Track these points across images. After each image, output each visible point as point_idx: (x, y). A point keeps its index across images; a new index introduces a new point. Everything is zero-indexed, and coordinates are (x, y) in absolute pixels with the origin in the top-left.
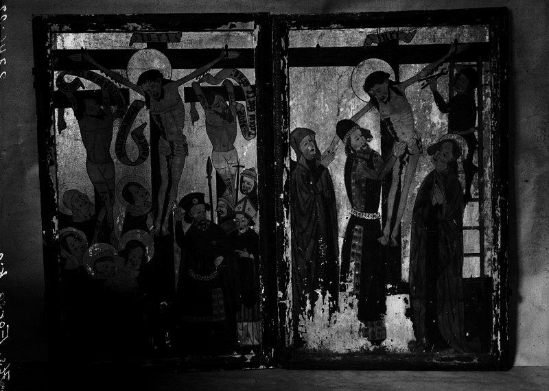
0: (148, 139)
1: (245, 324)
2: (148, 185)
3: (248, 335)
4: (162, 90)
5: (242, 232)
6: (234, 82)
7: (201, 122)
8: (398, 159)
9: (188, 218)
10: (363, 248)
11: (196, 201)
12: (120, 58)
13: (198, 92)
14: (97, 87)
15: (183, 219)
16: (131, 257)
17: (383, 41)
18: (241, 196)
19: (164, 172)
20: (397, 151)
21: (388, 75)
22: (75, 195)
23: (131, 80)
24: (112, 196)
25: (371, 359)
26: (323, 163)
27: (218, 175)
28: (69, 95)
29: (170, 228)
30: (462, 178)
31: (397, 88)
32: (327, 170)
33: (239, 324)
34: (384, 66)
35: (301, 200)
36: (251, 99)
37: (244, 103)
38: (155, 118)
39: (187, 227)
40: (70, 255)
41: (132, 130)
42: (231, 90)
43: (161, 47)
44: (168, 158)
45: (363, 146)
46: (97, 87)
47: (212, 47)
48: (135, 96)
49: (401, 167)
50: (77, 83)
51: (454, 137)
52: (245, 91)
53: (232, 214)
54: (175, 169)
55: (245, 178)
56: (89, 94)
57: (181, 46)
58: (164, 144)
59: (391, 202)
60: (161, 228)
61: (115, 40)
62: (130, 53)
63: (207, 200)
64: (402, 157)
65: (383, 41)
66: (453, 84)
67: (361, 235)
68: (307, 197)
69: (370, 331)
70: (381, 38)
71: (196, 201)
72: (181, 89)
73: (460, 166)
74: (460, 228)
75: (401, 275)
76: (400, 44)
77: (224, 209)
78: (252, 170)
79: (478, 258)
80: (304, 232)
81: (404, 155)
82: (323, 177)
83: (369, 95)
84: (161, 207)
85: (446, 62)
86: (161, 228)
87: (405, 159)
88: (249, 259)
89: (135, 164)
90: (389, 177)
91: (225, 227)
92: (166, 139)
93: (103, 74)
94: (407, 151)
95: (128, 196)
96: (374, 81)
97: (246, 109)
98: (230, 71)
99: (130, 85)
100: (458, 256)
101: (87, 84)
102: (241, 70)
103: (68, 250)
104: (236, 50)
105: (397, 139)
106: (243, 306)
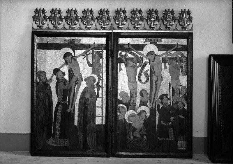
0: (149, 75)
1: (181, 142)
2: (148, 91)
3: (182, 146)
4: (155, 58)
5: (181, 108)
6: (180, 56)
7: (168, 69)
8: (74, 82)
9: (162, 103)
10: (62, 113)
11: (164, 97)
12: (140, 47)
13: (167, 59)
14: (133, 57)
15: (160, 103)
16: (141, 116)
17: (70, 42)
18: (181, 96)
19: (154, 86)
20: (74, 79)
21: (72, 54)
22: (124, 94)
23: (144, 55)
24: (136, 94)
25: (99, 154)
26: (48, 83)
27: (173, 88)
28: (123, 59)
29: (155, 106)
30: (96, 90)
31: (74, 58)
32: (50, 86)
33: (178, 142)
34: (70, 50)
35: (40, 95)
36: (185, 62)
37: (183, 63)
38: (152, 67)
39: (161, 106)
40: (121, 114)
41: (144, 71)
42: (178, 59)
43: (155, 44)
44: (156, 82)
45: (63, 78)
46: (133, 57)
47: (172, 44)
48: (145, 60)
49: (75, 85)
50: (126, 55)
51: (93, 75)
52: (183, 60)
53: (177, 103)
54: (158, 86)
55: (182, 90)
56: (131, 59)
57: (162, 43)
58: (154, 78)
60: (152, 106)
61: (140, 41)
62: (144, 45)
63: (169, 97)
64: (76, 82)
65: (70, 42)
66: (93, 57)
67: (61, 109)
68: (42, 95)
69: (63, 143)
70: (69, 41)
71: (164, 97)
72: (161, 58)
73: (95, 86)
74: (94, 106)
75: (74, 123)
76: (76, 43)
77: (174, 100)
78: (185, 87)
79: (101, 118)
80: (41, 107)
81: (76, 81)
82: (48, 88)
83: (65, 60)
84: (152, 99)
85: (91, 49)
86: (152, 106)
87: (77, 83)
88: (183, 118)
89: (144, 83)
90: (71, 88)
91: (175, 106)
92: (155, 75)
93: (135, 52)
94: (77, 80)
95: (141, 94)
96: (66, 55)
97: (183, 65)
98: (178, 52)
99: (144, 56)
100: (94, 116)
101: (130, 56)
102: (182, 52)
103: (120, 112)
104: (180, 45)
105: (74, 76)
106: (180, 135)
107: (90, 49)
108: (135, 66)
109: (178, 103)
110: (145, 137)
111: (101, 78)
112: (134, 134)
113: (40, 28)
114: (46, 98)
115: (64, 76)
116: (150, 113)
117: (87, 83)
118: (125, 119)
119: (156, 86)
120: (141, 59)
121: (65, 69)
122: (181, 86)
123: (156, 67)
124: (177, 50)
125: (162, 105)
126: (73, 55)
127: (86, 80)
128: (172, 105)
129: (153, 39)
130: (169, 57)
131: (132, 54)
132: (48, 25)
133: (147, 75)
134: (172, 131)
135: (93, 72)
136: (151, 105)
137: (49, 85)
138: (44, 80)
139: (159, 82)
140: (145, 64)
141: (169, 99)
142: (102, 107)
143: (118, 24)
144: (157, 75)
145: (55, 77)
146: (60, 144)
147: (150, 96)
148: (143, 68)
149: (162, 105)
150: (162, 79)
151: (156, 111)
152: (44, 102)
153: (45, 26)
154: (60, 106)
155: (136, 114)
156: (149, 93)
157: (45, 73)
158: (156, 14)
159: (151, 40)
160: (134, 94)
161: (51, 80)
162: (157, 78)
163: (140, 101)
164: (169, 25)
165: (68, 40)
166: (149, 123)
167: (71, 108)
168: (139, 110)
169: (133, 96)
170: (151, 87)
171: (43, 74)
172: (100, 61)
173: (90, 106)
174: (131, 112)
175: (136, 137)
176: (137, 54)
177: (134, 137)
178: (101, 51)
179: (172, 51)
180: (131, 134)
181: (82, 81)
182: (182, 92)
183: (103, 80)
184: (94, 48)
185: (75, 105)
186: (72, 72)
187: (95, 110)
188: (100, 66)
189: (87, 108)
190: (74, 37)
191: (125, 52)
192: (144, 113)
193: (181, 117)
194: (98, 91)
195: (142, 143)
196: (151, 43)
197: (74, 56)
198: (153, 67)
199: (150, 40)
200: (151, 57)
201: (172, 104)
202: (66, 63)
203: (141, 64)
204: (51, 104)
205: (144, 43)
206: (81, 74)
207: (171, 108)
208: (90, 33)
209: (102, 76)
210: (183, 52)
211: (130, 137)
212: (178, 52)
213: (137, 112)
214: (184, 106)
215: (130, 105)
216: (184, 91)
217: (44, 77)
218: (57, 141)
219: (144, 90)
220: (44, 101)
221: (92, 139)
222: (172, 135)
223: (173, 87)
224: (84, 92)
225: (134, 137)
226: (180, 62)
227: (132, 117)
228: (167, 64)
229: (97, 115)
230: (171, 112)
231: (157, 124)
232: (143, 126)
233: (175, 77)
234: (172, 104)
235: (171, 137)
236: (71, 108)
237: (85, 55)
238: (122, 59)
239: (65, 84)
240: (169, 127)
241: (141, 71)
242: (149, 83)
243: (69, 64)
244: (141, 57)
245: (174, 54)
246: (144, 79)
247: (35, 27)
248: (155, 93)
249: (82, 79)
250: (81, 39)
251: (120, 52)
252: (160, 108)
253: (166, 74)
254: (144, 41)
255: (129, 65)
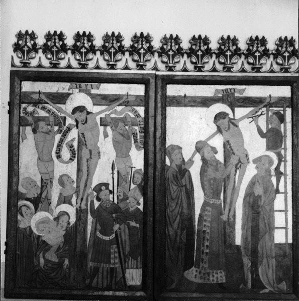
1: (132, 270)
2: (74, 177)
5: (132, 209)
9: (98, 199)
11: (103, 188)
12: (61, 98)
14: (47, 115)
15: (95, 198)
19: (84, 168)
20: (234, 160)
24: (52, 182)
26: (186, 167)
27: (118, 172)
28: (30, 119)
29: (87, 205)
30: (274, 180)
31: (233, 123)
32: (189, 171)
33: (127, 270)
37: (137, 128)
38: (81, 135)
39: (97, 204)
41: (66, 142)
42: (129, 119)
46: (47, 115)
48: (70, 121)
49: (236, 171)
53: (126, 198)
54: (91, 167)
55: (136, 175)
58: (85, 153)
59: (229, 192)
60: (81, 204)
62: (68, 95)
63: (111, 188)
64: (237, 165)
67: (210, 214)
70: (225, 91)
71: (103, 188)
74: (272, 210)
77: (120, 194)
80: (173, 211)
82: (186, 175)
84: (81, 191)
85: (264, 107)
86: (81, 204)
88: (135, 227)
89: (67, 163)
90: (229, 176)
91: (122, 205)
92: (87, 148)
95: (61, 182)
96: (219, 117)
97: (138, 132)
98: (129, 108)
100: (271, 228)
101: (43, 114)
102: (135, 107)
103: (22, 215)
105: (234, 154)
107: (262, 106)
108: (50, 131)
109: (127, 199)
110: (67, 262)
111: (281, 159)
112: (47, 255)
113: (25, 65)
114: (183, 195)
115: (215, 155)
116: (77, 218)
117: (257, 168)
118: (30, 227)
119: (88, 168)
120: (61, 119)
121: (218, 142)
122: (133, 168)
123: (90, 133)
124: (127, 104)
125: (99, 203)
126: (232, 117)
127: (255, 161)
128: (116, 203)
129: (83, 85)
130: (113, 116)
131: (46, 110)
132: (40, 60)
133: (72, 149)
134: (116, 250)
135: (269, 148)
136: (79, 203)
137: (187, 170)
138: (179, 162)
139: (93, 161)
140: (69, 129)
141: (112, 192)
142: (286, 211)
143: (21, 58)
144: (89, 147)
145: (198, 157)
146: (208, 279)
147: (78, 187)
148: (65, 135)
149: (99, 203)
150: (100, 156)
151: (87, 213)
152: (179, 202)
153: (34, 63)
154: (208, 208)
155: (50, 218)
156: (75, 180)
157: (181, 148)
158: (89, 40)
159: (80, 87)
160: (49, 182)
161: (191, 161)
162: (91, 154)
163: (58, 194)
164: (112, 60)
165: (223, 90)
166: (73, 234)
167: (229, 212)
168: (57, 212)
169: (46, 186)
170: (79, 170)
171: (177, 151)
172: (281, 127)
173: (264, 209)
174: (41, 215)
175: (50, 261)
176: (54, 110)
177: (46, 261)
178: (282, 109)
179: (118, 105)
180: (41, 255)
181: (249, 163)
182: (136, 179)
183: (287, 161)
184: (270, 104)
185: (237, 207)
186: (230, 147)
187: (273, 217)
188: (282, 137)
189: (258, 211)
190: (232, 85)
191: (33, 106)
192: (66, 216)
193: (133, 224)
194: (278, 181)
195: (60, 272)
196: (80, 92)
197: (234, 119)
198: (83, 134)
199: (78, 86)
200: (81, 116)
201: (116, 201)
202: (219, 130)
203: (60, 129)
204: (191, 205)
205: (67, 91)
206: (246, 150)
207: (116, 209)
208: (187, 77)
209: (285, 155)
210: (137, 108)
211: (39, 261)
212: (128, 107)
213: (52, 215)
214: (139, 204)
215: (39, 202)
216: (139, 178)
217: (178, 156)
218: (204, 274)
219: (67, 175)
220: (180, 201)
221: (267, 270)
222: (116, 257)
223: (120, 171)
224: (252, 184)
225: (46, 261)
226: (133, 125)
227: (43, 224)
228: (108, 129)
229: (276, 225)
230: (114, 215)
231: (89, 237)
232: (63, 240)
233: (122, 152)
234: (116, 201)
235: (115, 261)
236: (229, 212)
237: (254, 117)
238: (26, 119)
239: (217, 170)
240: (111, 242)
241: (61, 141)
242: (76, 164)
243: (224, 132)
244: (63, 115)
245: (121, 113)
246: (66, 154)
247: (17, 62)
248: (87, 179)
249: (248, 159)
250: (245, 88)
251: (23, 106)
252: (96, 208)
253: (106, 147)
254: (68, 87)
255: (40, 129)
